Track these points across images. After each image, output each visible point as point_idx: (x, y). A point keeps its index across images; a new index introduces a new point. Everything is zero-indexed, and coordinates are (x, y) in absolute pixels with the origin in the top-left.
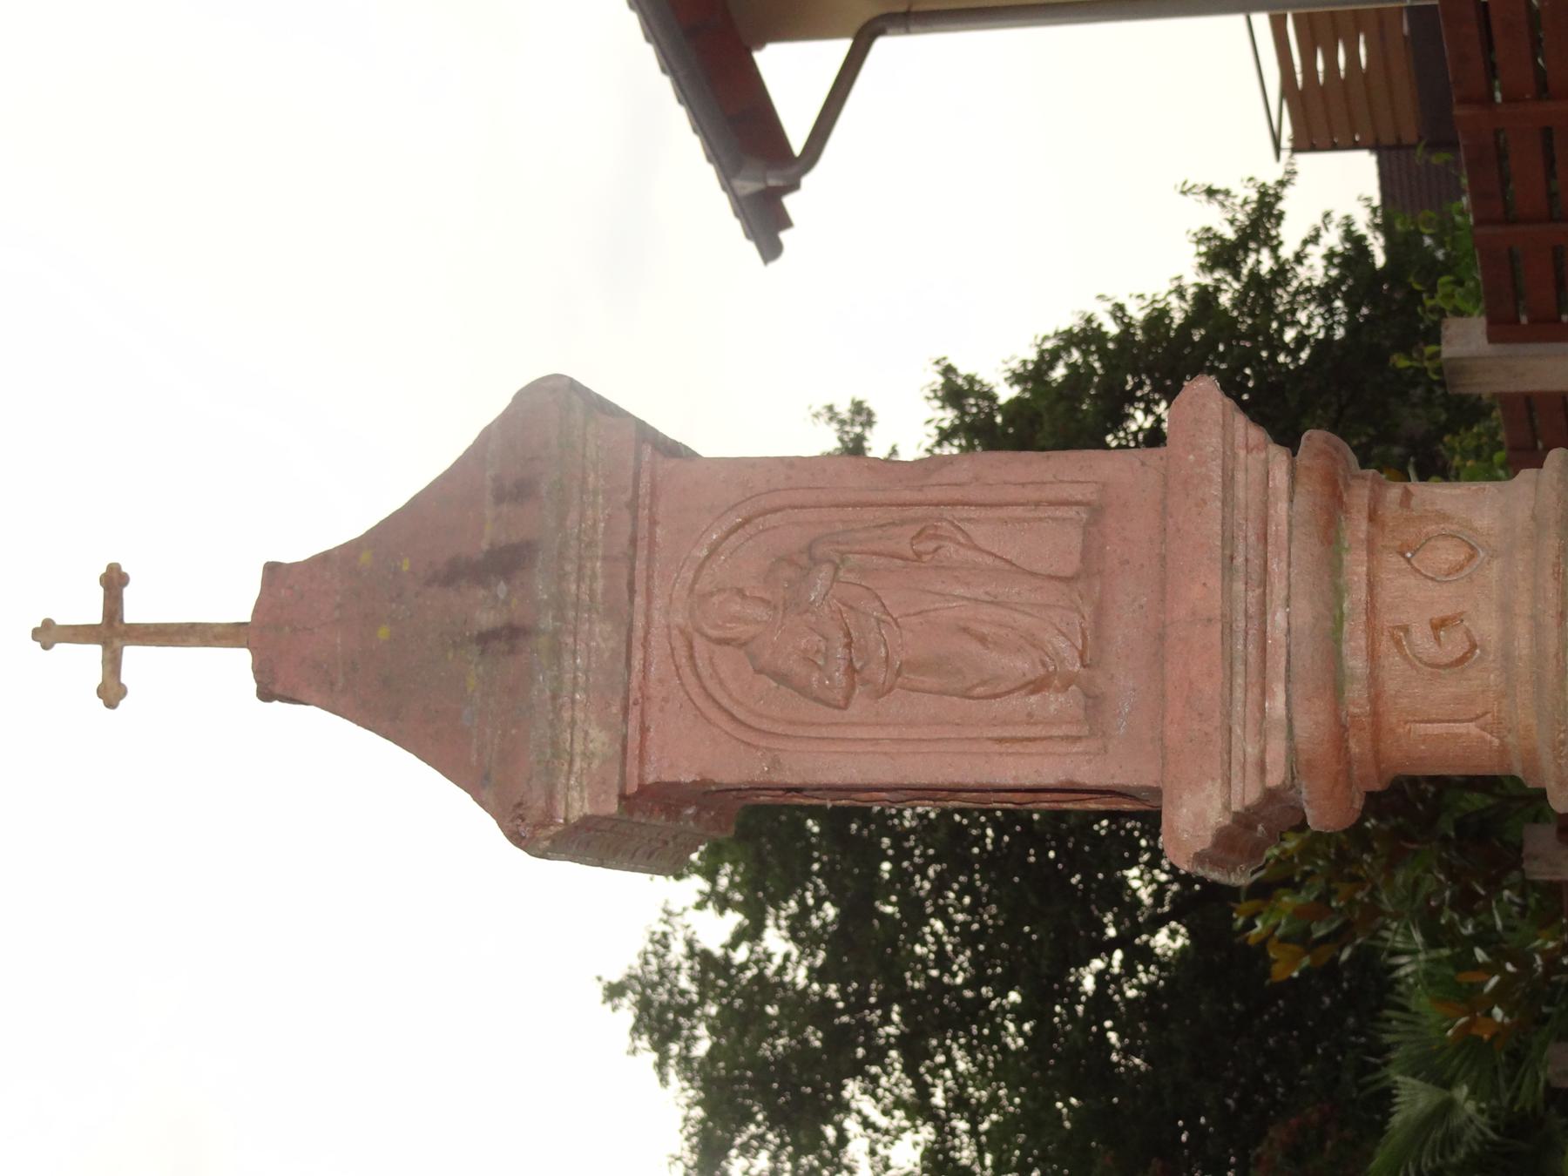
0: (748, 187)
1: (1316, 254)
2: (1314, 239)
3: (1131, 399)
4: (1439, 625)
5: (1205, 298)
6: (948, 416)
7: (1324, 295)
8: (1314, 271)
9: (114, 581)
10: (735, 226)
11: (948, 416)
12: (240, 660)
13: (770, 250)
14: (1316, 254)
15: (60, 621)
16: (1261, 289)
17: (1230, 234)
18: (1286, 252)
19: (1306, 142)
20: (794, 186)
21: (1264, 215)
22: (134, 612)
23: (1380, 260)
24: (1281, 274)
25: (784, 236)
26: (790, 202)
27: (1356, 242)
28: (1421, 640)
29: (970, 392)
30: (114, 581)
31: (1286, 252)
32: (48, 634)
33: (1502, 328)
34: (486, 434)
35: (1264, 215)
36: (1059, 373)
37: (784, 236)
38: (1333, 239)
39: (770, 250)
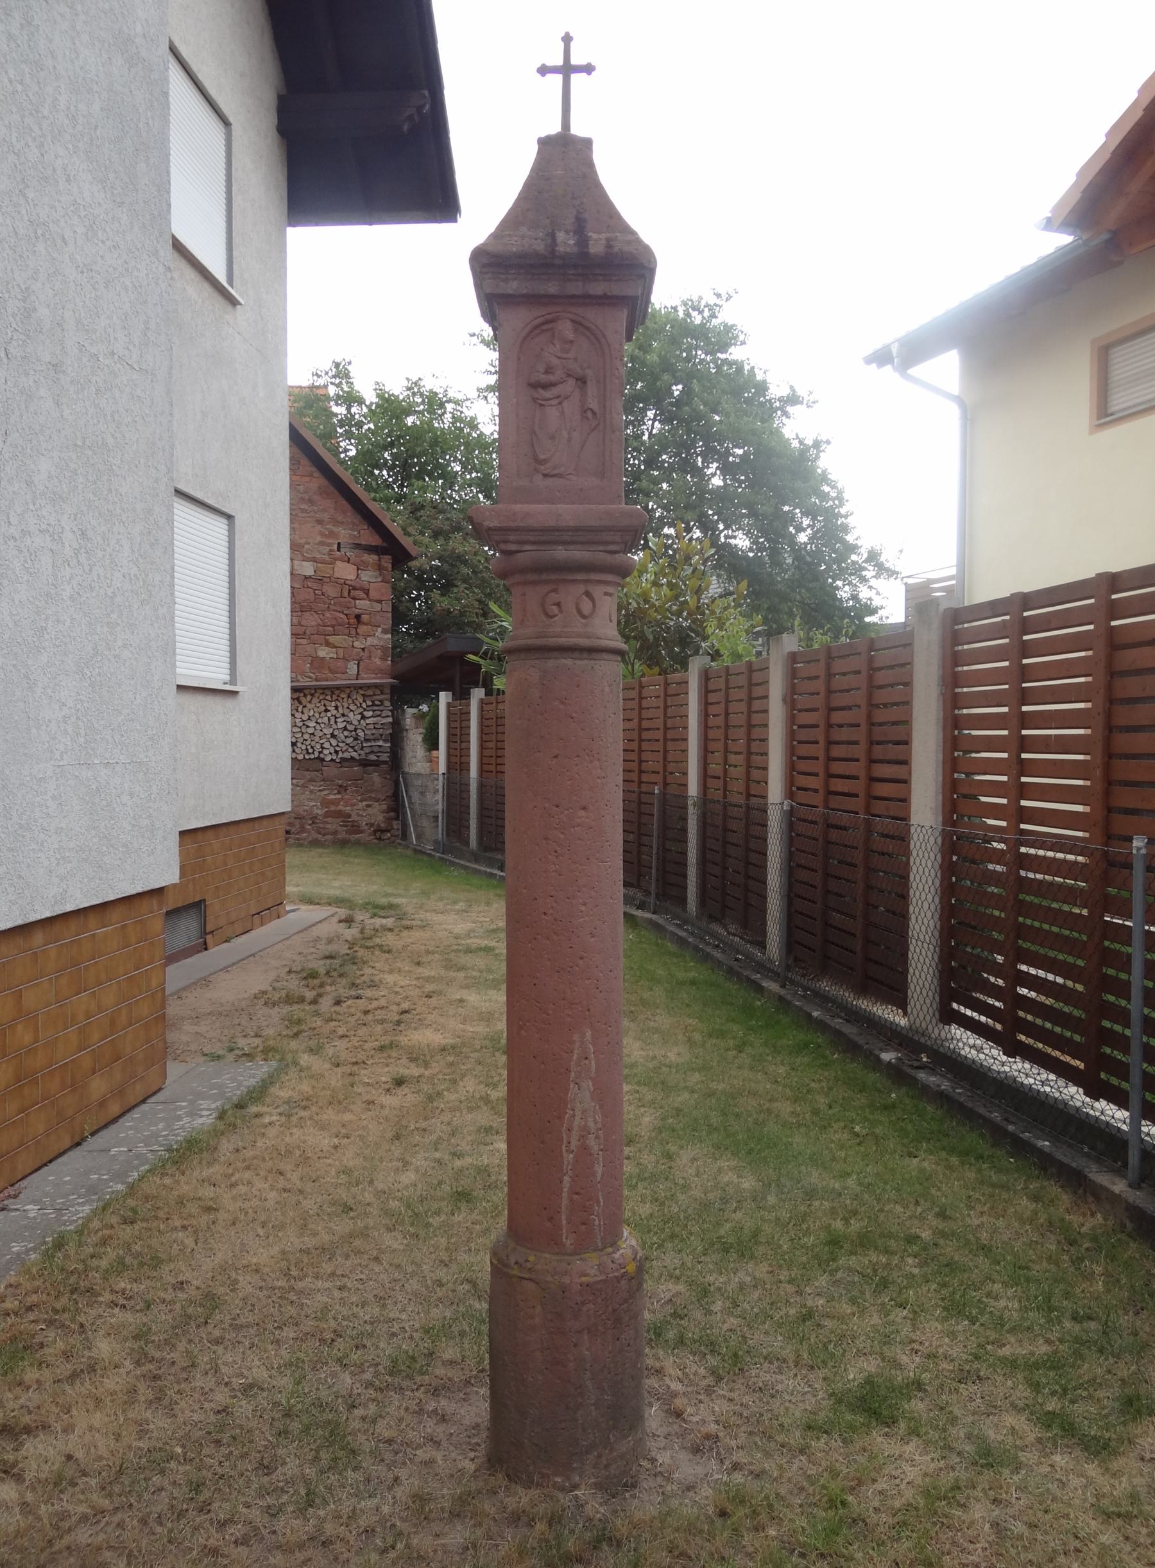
0: (895, 350)
1: (872, 594)
2: (878, 593)
3: (814, 519)
4: (558, 604)
5: (854, 548)
6: (809, 442)
7: (855, 597)
8: (864, 594)
9: (588, 69)
10: (879, 346)
11: (809, 442)
12: (555, 128)
13: (869, 360)
14: (872, 594)
15: (572, 44)
16: (858, 570)
17: (882, 559)
18: (873, 582)
19: (909, 589)
20: (895, 369)
21: (883, 570)
22: (575, 78)
23: (867, 619)
24: (864, 580)
25: (874, 365)
26: (889, 367)
27: (873, 611)
28: (554, 597)
29: (819, 452)
30: (588, 69)
31: (873, 582)
32: (567, 39)
33: (793, 657)
34: (633, 233)
35: (883, 570)
36: (826, 489)
37: (874, 365)
38: (876, 602)
39: (869, 360)
